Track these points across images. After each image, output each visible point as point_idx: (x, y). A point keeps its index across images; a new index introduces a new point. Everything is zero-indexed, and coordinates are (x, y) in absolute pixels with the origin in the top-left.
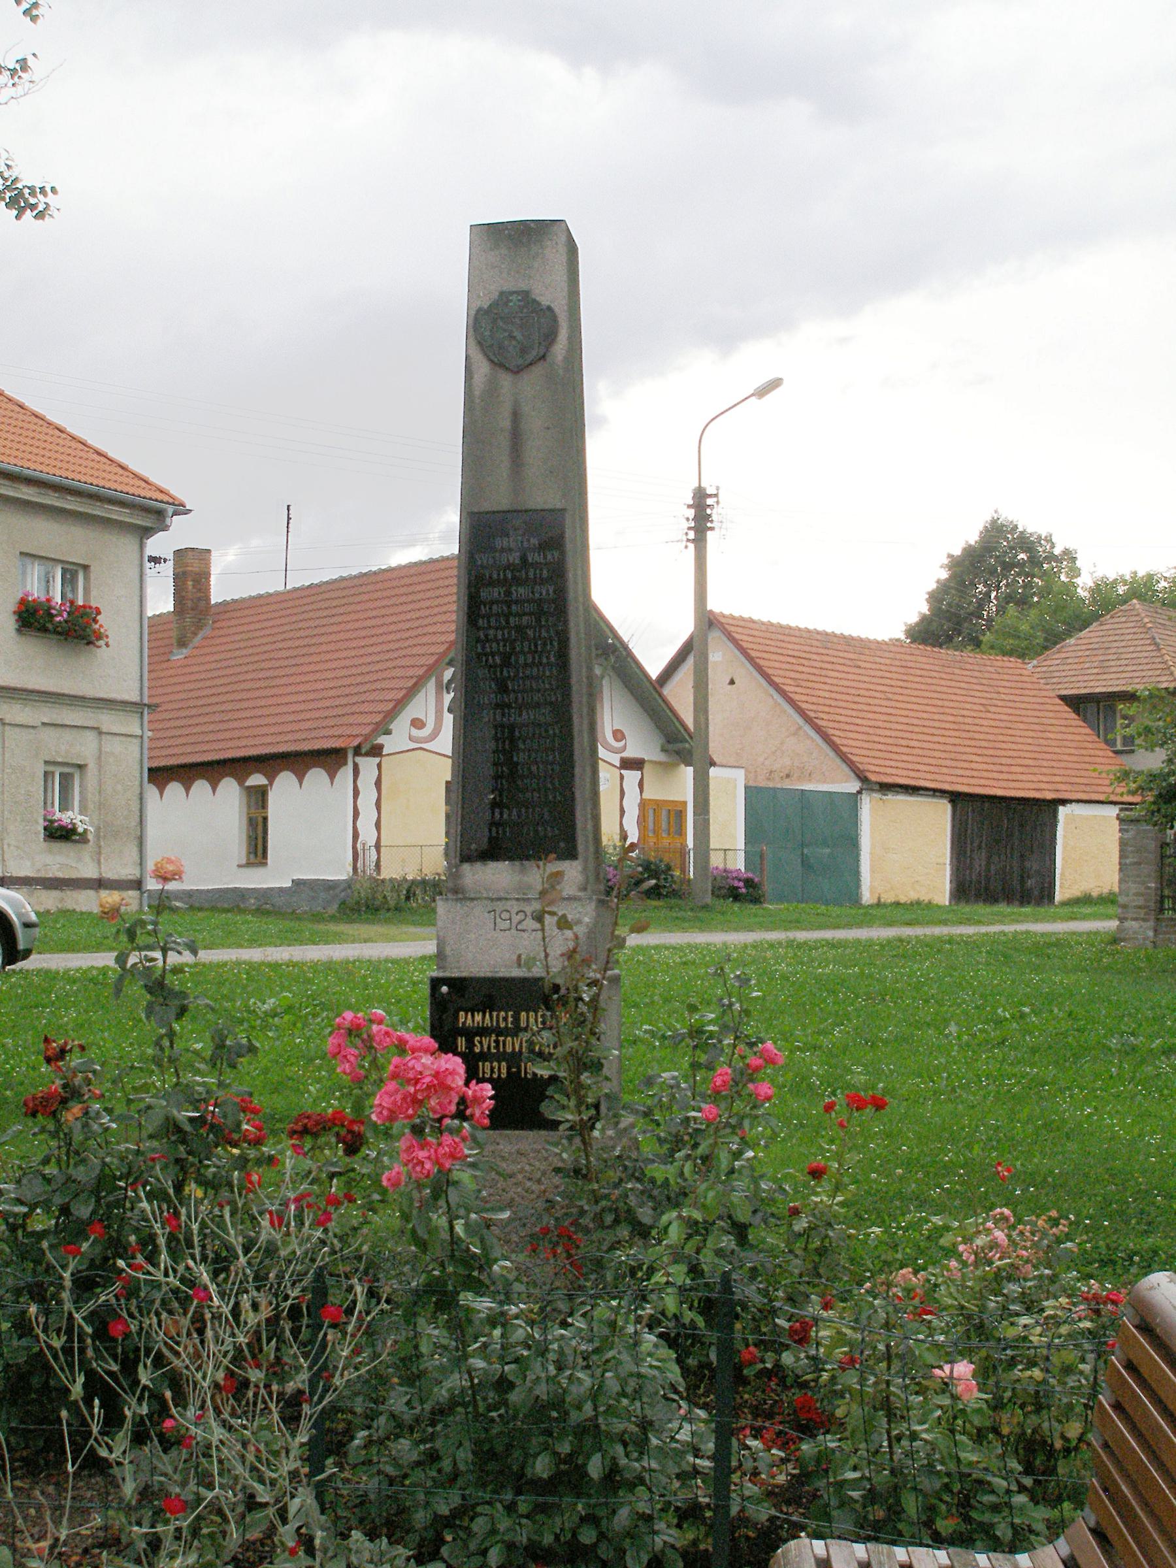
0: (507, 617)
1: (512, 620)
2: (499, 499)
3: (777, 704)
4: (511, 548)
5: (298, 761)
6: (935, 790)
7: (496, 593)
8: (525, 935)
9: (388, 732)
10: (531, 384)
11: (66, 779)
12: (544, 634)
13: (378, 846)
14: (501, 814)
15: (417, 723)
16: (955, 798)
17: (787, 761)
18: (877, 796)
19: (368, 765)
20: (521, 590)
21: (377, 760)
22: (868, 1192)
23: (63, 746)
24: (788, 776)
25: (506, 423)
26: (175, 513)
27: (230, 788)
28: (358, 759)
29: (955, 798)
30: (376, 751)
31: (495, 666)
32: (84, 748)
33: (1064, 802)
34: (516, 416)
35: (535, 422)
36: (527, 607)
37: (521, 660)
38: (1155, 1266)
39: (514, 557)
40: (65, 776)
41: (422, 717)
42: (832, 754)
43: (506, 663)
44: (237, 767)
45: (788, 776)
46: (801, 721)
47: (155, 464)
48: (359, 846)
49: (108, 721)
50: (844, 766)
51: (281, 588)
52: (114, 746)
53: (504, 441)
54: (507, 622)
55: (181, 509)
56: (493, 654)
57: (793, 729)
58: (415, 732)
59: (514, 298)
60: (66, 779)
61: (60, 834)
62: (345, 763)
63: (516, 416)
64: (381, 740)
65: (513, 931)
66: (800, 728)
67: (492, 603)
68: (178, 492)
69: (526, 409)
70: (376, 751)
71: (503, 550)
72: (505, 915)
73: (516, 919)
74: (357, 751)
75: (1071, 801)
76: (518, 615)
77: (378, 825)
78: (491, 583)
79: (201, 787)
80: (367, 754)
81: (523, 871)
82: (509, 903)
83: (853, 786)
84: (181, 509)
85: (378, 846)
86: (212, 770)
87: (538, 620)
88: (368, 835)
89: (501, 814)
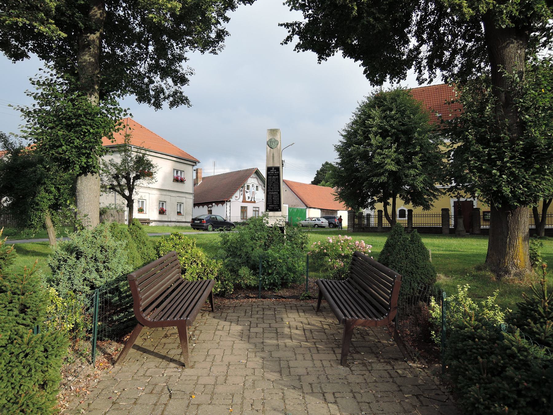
2: (270, 166)
5: (217, 203)
10: (274, 151)
11: (180, 205)
15: (236, 197)
16: (321, 209)
19: (228, 203)
22: (519, 286)
23: (180, 200)
27: (206, 207)
29: (321, 209)
30: (230, 201)
32: (183, 200)
35: (276, 155)
38: (385, 251)
40: (180, 204)
44: (207, 204)
47: (196, 157)
49: (187, 196)
52: (188, 200)
55: (199, 162)
60: (180, 205)
61: (179, 213)
68: (198, 159)
70: (230, 201)
74: (227, 201)
79: (201, 207)
83: (305, 207)
84: (199, 162)
86: (203, 204)
88: (228, 215)
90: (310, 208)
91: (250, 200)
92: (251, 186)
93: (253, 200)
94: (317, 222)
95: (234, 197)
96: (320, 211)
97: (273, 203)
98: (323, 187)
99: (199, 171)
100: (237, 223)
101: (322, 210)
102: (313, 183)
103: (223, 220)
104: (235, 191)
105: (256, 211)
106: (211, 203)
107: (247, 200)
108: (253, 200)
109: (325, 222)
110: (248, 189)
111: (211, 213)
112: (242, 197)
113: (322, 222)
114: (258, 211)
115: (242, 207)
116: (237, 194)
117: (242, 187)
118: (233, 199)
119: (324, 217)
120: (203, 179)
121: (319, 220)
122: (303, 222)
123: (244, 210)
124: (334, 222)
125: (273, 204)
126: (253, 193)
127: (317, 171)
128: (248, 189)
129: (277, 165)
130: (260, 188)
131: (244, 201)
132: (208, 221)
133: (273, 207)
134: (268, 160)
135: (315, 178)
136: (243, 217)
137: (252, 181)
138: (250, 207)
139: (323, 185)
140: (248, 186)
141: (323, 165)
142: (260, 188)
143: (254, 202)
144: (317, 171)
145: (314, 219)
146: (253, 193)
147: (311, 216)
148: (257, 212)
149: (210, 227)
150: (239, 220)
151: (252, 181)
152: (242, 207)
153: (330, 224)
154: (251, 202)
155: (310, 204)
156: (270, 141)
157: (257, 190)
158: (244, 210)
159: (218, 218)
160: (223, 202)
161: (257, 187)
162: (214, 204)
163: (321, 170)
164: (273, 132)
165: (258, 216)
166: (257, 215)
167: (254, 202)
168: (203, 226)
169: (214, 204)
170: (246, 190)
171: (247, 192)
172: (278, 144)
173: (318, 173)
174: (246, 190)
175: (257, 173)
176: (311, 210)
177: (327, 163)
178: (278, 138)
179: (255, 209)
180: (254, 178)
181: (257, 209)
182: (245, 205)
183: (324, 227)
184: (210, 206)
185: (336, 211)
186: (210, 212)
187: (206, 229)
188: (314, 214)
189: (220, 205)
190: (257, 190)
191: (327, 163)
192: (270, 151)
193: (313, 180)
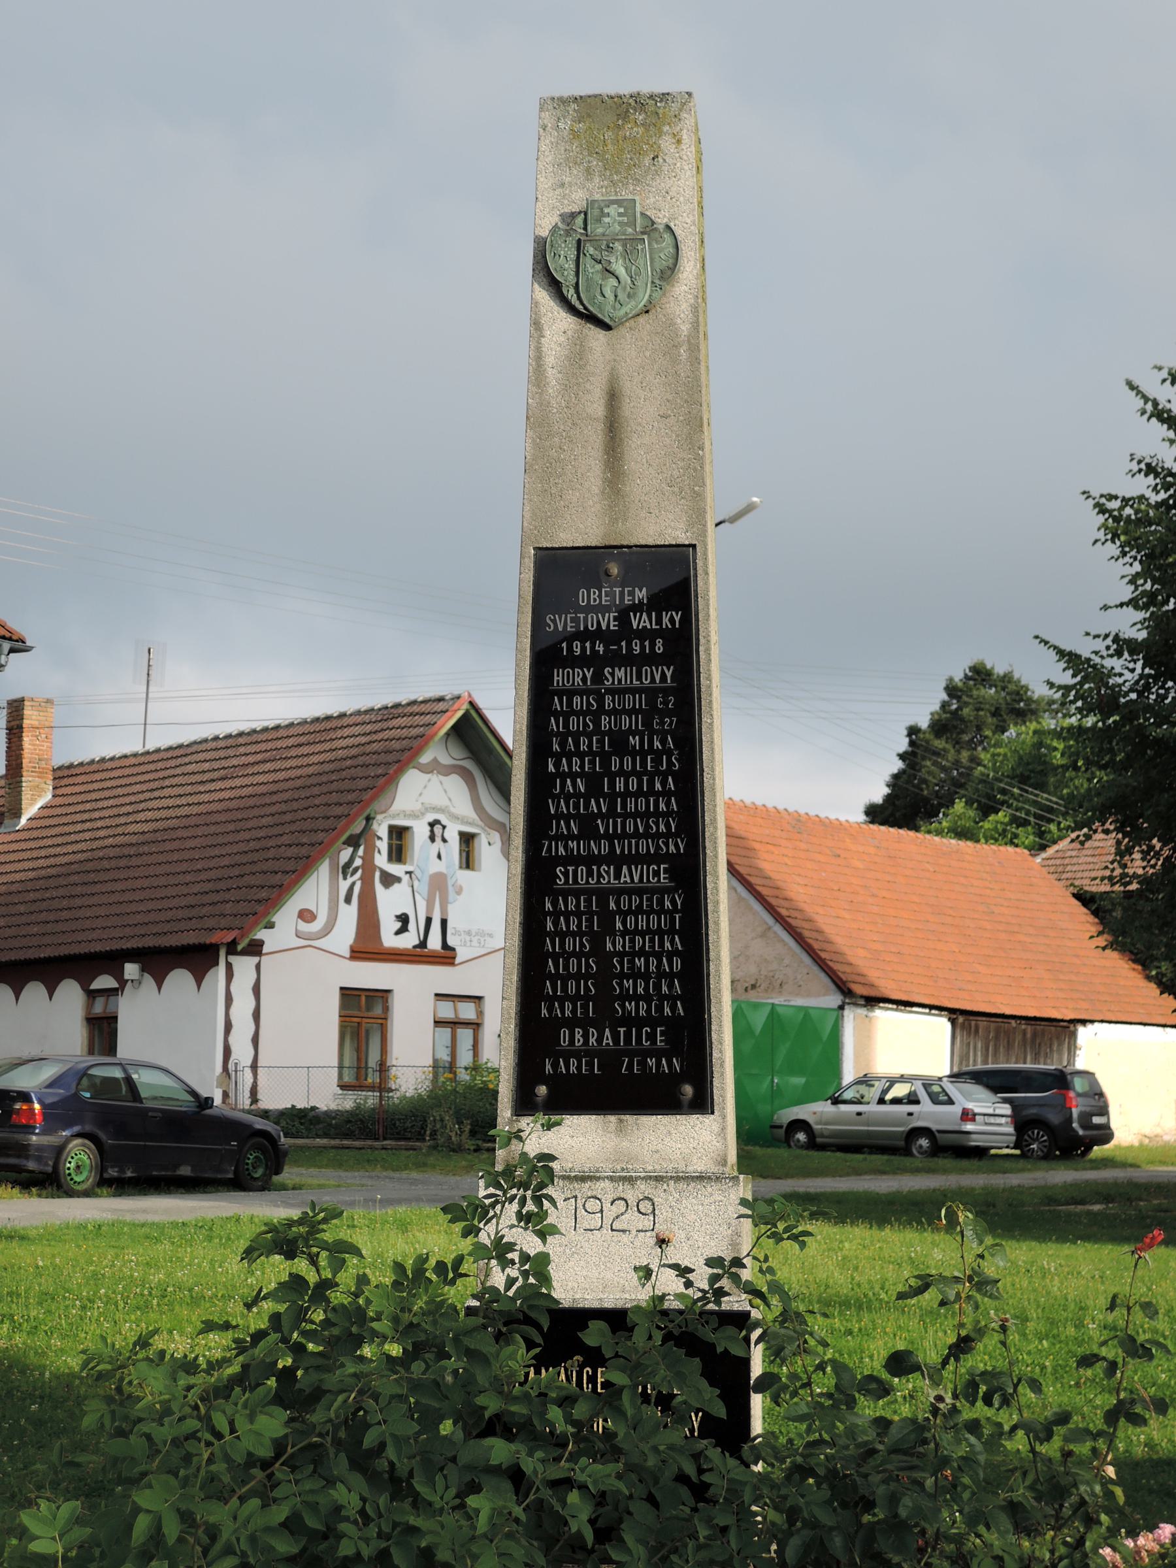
0: (596, 716)
1: (604, 720)
2: (582, 528)
3: (741, 899)
4: (598, 606)
5: (159, 961)
6: (931, 1007)
7: (578, 677)
8: (625, 1238)
9: (271, 926)
10: (628, 352)
12: (657, 744)
13: (254, 1067)
14: (586, 1036)
15: (306, 915)
16: (954, 1014)
17: (753, 969)
18: (862, 1011)
19: (244, 966)
20: (620, 673)
21: (256, 959)
24: (754, 987)
25: (597, 407)
26: (12, 651)
27: (70, 994)
28: (232, 959)
30: (255, 948)
31: (577, 795)
33: (1084, 1022)
34: (613, 397)
35: (645, 409)
36: (629, 701)
37: (620, 785)
39: (608, 621)
41: (313, 908)
42: (807, 960)
43: (594, 789)
45: (754, 987)
46: (770, 920)
48: (231, 1066)
50: (822, 975)
51: (139, 749)
53: (595, 436)
54: (597, 724)
56: (574, 776)
57: (760, 930)
58: (304, 927)
59: (612, 210)
62: (216, 963)
63: (613, 397)
64: (261, 934)
65: (606, 1231)
66: (770, 928)
67: (571, 693)
69: (630, 387)
70: (255, 948)
71: (589, 609)
72: (593, 1205)
73: (611, 1211)
74: (232, 949)
75: (1092, 1022)
76: (614, 712)
77: (255, 1041)
78: (573, 662)
79: (35, 991)
80: (244, 953)
81: (620, 1130)
82: (602, 1184)
85: (254, 1067)
86: (48, 970)
87: (647, 724)
88: (242, 1053)
89: (586, 1036)
90: (872, 1001)
91: (408, 941)
92: (420, 831)
93: (434, 943)
94: (928, 1114)
95: (286, 918)
96: (943, 1025)
97: (604, 998)
98: (966, 846)
99: (30, 717)
100: (302, 1120)
101: (963, 1019)
102: (875, 814)
103: (185, 1102)
104: (297, 870)
105: (457, 1020)
106: (112, 961)
107: (390, 939)
108: (434, 943)
109: (989, 1116)
110: (398, 853)
111: (110, 1047)
112: (349, 916)
113: (967, 1116)
114: (476, 1026)
115: (349, 995)
116: (316, 890)
117: (354, 842)
118: (281, 931)
119: (978, 1077)
120: (64, 775)
121: (941, 1098)
122: (817, 1111)
123: (363, 1013)
124: (1054, 1118)
125: (604, 1018)
126: (439, 884)
127: (913, 731)
128: (398, 853)
129: (659, 527)
130: (489, 850)
131: (367, 948)
132: (63, 1112)
133: (611, 1059)
134: (544, 469)
135: (896, 781)
136: (360, 1068)
137: (430, 795)
138: (412, 993)
139: (962, 834)
140: (399, 834)
141: (952, 690)
142: (489, 850)
143: (447, 956)
144: (913, 731)
145: (900, 1090)
146: (439, 884)
147: (885, 1064)
148: (465, 1035)
149: (79, 1158)
150: (324, 1093)
151: (430, 795)
152: (349, 995)
153: (1024, 1124)
154: (419, 955)
155: (873, 975)
156: (580, 227)
157: (468, 861)
158: (363, 1013)
159: (142, 1078)
160: (199, 958)
161: (467, 839)
162: (131, 970)
163: (940, 726)
164: (619, 126)
165: (475, 1068)
166: (465, 1058)
167: (447, 956)
168: (23, 1150)
169: (131, 970)
170: (381, 860)
171: (389, 880)
172: (668, 274)
173: (918, 748)
174: (381, 860)
175: (471, 733)
176: (884, 1017)
177: (980, 674)
178: (670, 197)
179: (446, 1011)
180: (447, 771)
181: (467, 1012)
182: (370, 975)
183: (980, 1153)
184: (105, 982)
185: (1061, 1031)
186: (103, 1031)
187: (49, 1181)
188: (904, 1048)
189: (180, 979)
190: (468, 861)
191: (980, 674)
192: (577, 355)
193: (878, 793)
